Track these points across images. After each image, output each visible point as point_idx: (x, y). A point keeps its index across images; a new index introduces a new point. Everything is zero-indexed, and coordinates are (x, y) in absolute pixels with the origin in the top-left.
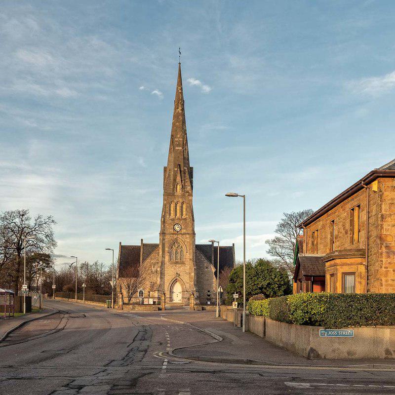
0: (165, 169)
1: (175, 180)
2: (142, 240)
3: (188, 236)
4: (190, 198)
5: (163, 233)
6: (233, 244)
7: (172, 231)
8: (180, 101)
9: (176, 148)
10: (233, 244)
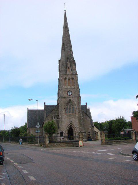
0: (59, 61)
1: (67, 66)
2: (45, 103)
3: (76, 98)
4: (76, 76)
5: (59, 97)
6: (86, 103)
7: (66, 95)
8: (66, 27)
9: (66, 49)
10: (86, 103)
